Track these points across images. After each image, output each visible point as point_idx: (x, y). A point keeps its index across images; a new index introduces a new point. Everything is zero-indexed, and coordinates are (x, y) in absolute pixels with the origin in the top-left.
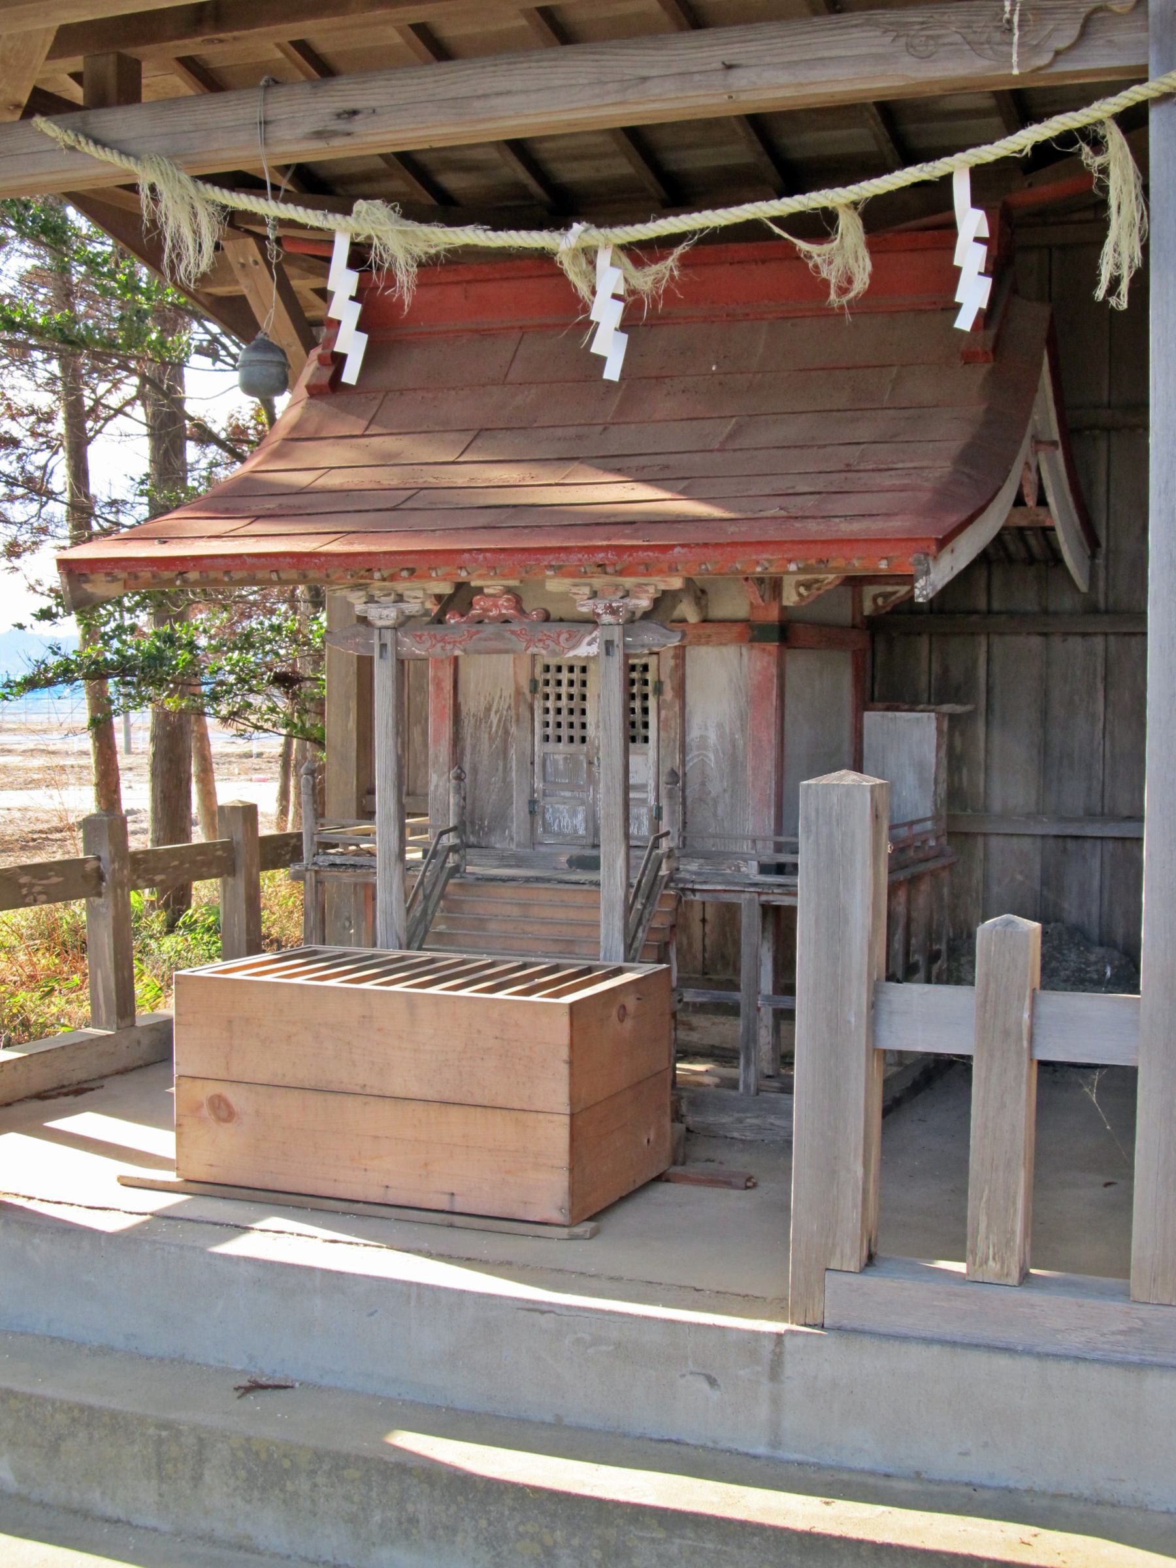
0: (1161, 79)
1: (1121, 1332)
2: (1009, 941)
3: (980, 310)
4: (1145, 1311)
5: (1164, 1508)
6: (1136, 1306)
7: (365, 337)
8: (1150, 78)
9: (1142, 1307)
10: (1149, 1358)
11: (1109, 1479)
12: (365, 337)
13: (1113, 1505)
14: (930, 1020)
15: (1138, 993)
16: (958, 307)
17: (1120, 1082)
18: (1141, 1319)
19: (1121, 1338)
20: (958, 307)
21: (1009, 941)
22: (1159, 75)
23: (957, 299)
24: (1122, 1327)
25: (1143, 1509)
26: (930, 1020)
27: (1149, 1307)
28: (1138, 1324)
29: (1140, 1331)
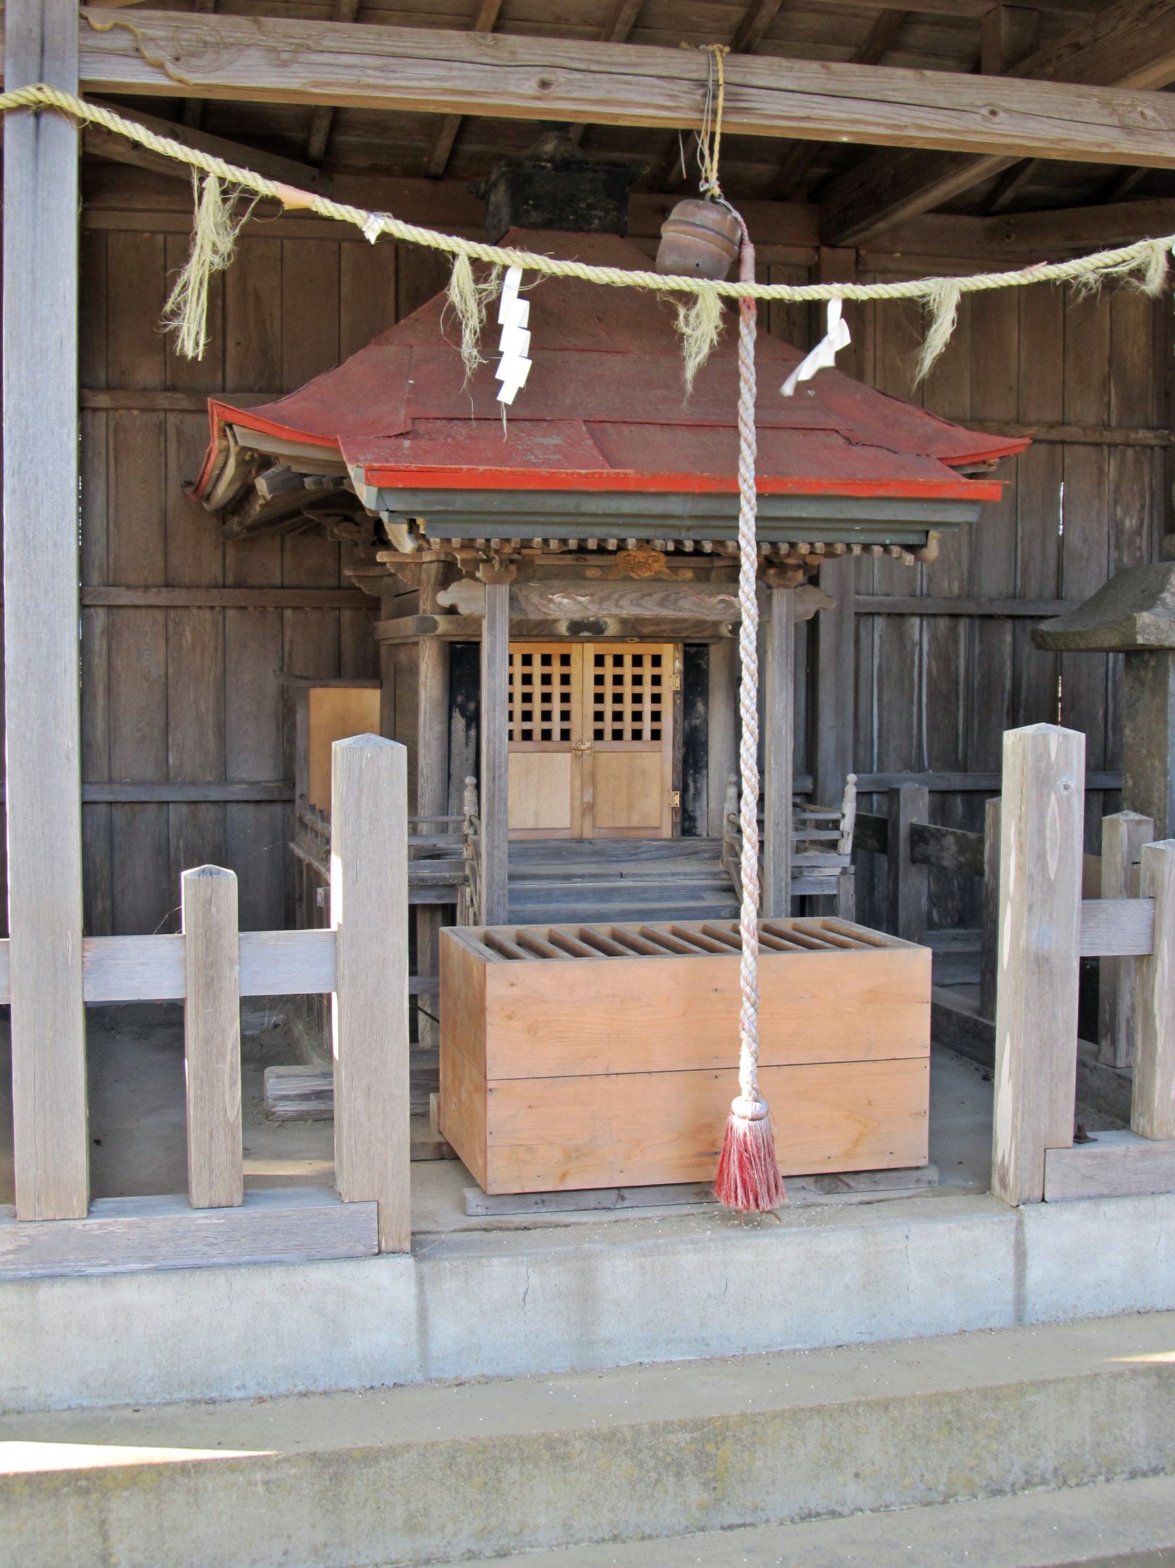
0: (19, 92)
1: (10, 1252)
2: (209, 892)
3: (520, 390)
4: (31, 1229)
5: (65, 1406)
6: (22, 1225)
7: (497, 376)
8: (6, 89)
9: (29, 1225)
10: (38, 1272)
11: (13, 1389)
12: (497, 376)
13: (19, 1413)
14: (142, 968)
15: (7, 936)
16: (500, 383)
17: (313, 1009)
18: (29, 1236)
19: (11, 1257)
20: (500, 383)
21: (209, 892)
22: (14, 88)
23: (498, 376)
24: (11, 1247)
25: (46, 1410)
26: (142, 968)
27: (35, 1224)
28: (25, 1241)
29: (28, 1247)
